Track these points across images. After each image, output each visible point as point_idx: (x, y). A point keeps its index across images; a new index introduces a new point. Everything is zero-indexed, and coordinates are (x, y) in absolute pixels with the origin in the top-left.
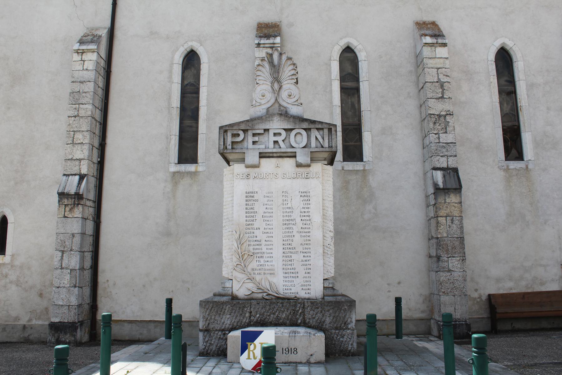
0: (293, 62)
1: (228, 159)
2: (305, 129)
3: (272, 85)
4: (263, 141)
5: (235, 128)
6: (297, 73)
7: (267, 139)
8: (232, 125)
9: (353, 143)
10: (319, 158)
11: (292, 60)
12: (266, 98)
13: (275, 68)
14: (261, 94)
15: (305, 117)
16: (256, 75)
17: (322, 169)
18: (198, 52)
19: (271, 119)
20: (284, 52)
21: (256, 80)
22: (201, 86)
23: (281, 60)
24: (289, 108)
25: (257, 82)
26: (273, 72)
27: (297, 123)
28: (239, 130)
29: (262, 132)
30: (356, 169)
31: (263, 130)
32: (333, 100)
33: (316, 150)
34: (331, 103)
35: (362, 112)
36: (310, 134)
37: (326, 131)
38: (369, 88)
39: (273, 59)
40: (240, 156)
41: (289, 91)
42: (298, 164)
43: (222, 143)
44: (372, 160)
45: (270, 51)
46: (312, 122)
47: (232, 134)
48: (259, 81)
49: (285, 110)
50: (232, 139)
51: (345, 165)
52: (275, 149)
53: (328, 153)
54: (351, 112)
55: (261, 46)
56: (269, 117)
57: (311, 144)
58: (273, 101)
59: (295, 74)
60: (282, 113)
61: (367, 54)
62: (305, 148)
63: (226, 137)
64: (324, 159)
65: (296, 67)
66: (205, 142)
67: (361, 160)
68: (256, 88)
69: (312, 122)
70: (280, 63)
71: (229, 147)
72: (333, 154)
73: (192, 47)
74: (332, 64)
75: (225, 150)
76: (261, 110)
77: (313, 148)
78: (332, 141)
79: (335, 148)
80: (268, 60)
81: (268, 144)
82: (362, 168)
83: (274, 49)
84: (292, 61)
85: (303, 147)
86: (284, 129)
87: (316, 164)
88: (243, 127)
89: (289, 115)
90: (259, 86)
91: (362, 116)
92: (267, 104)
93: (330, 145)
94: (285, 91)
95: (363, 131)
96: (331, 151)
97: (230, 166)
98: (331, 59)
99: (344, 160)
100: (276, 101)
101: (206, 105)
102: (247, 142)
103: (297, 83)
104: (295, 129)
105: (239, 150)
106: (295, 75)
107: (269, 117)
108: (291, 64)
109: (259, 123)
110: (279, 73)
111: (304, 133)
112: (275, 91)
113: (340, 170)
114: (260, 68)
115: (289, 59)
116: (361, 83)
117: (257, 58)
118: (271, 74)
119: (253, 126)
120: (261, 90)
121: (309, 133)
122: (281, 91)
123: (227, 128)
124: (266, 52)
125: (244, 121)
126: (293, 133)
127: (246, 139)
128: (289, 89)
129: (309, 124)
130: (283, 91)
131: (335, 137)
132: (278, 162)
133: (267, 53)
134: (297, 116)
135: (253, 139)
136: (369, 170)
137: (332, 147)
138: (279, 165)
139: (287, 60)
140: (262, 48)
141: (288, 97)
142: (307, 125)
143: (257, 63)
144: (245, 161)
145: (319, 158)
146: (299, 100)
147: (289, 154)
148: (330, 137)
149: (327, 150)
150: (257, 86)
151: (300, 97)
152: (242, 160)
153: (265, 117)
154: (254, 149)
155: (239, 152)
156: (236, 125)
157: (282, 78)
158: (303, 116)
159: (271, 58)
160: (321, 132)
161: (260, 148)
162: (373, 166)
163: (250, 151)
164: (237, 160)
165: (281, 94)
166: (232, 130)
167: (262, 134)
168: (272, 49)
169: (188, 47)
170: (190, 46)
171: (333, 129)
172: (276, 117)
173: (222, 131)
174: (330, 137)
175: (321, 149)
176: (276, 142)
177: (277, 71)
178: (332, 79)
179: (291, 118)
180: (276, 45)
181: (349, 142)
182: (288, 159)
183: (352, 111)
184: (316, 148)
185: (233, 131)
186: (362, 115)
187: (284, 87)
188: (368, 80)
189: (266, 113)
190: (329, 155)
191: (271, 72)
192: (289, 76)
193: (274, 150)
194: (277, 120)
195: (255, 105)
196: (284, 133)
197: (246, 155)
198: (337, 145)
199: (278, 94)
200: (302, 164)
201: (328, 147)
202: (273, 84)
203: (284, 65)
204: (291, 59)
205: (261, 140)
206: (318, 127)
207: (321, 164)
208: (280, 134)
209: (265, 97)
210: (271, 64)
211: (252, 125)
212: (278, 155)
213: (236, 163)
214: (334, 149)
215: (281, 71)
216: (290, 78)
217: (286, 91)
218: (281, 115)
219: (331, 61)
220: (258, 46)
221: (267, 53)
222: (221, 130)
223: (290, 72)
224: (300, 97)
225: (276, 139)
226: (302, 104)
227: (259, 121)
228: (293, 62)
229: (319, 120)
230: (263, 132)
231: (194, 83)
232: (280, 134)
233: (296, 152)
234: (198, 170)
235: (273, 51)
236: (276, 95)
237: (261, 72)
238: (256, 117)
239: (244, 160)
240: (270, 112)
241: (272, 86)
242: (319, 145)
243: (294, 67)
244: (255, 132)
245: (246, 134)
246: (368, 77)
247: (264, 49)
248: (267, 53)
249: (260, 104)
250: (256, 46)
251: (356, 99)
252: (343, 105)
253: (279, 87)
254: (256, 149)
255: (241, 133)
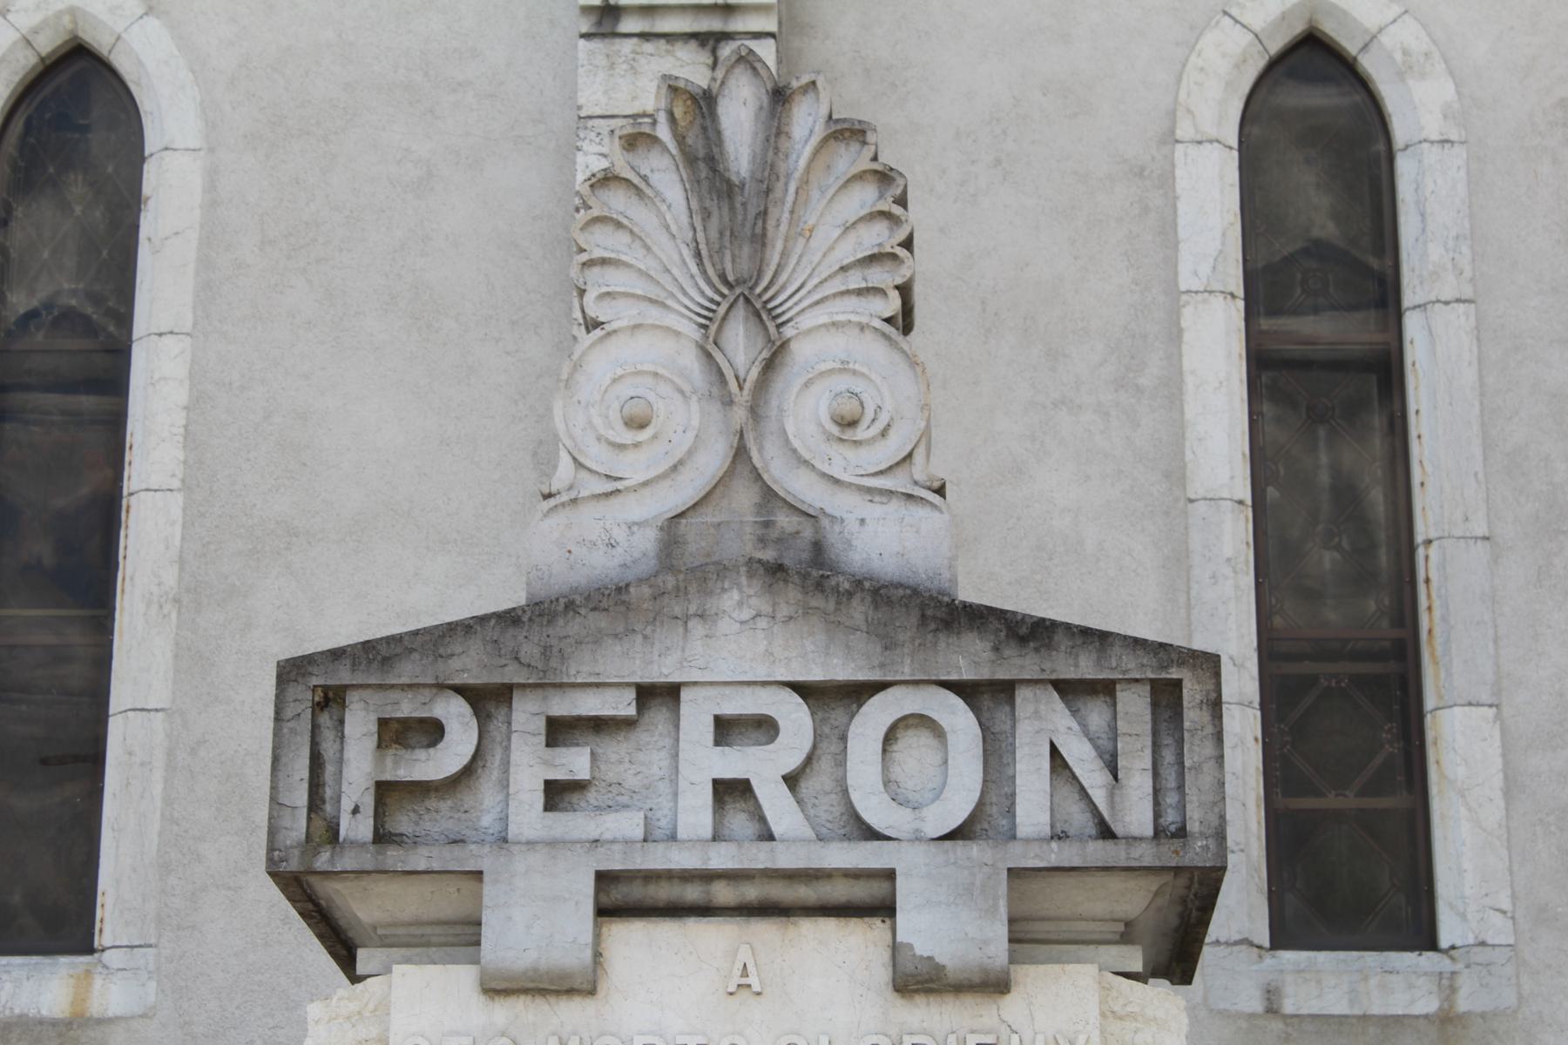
0: (875, 159)
1: (342, 923)
2: (965, 690)
3: (706, 337)
4: (632, 782)
5: (406, 671)
6: (908, 244)
7: (665, 763)
8: (384, 650)
9: (1348, 801)
10: (1081, 926)
11: (864, 143)
12: (655, 437)
13: (732, 208)
14: (616, 406)
15: (967, 593)
16: (584, 257)
17: (1103, 1015)
18: (122, 63)
19: (693, 609)
20: (805, 79)
21: (582, 292)
22: (140, 326)
23: (784, 144)
24: (842, 520)
25: (591, 313)
26: (714, 234)
27: (902, 637)
28: (441, 687)
29: (622, 705)
30: (1376, 1009)
31: (631, 695)
32: (1189, 456)
33: (1056, 855)
34: (1177, 474)
35: (1421, 552)
36: (1007, 727)
37: (1135, 706)
38: (1480, 360)
39: (719, 133)
40: (443, 902)
41: (842, 383)
42: (910, 968)
43: (301, 797)
44: (1511, 941)
45: (692, 67)
46: (1023, 631)
47: (383, 723)
48: (606, 303)
49: (808, 533)
50: (379, 762)
51: (1289, 978)
52: (722, 847)
53: (1154, 888)
54: (1338, 548)
55: (629, 25)
56: (680, 592)
57: (1011, 811)
58: (712, 461)
59: (894, 256)
60: (787, 562)
61: (1458, 93)
62: (1053, 769)
63: (329, 748)
64: (1121, 927)
65: (902, 201)
66: (158, 775)
67: (1424, 936)
68: (584, 354)
69: (1023, 631)
70: (772, 166)
71: (356, 828)
72: (1189, 888)
73: (75, 22)
74: (1178, 173)
75: (317, 853)
76: (620, 534)
77: (1027, 841)
78: (1181, 787)
79: (1212, 844)
80: (680, 139)
81: (666, 803)
82: (1427, 1004)
83: (727, 50)
84: (868, 152)
85: (951, 836)
86: (798, 687)
87: (1057, 967)
88: (470, 665)
89: (837, 571)
90: (601, 340)
91: (1427, 581)
92: (667, 483)
93: (1170, 817)
94: (807, 384)
95: (1430, 702)
96: (1177, 870)
97: (355, 979)
98: (1173, 132)
99: (1283, 936)
100: (739, 467)
101: (176, 484)
102: (504, 784)
103: (905, 321)
104: (881, 686)
105: (435, 851)
106: (889, 265)
107: (677, 588)
108: (860, 177)
109: (597, 640)
110: (760, 241)
111: (957, 717)
112: (733, 385)
113: (1252, 1016)
114: (616, 201)
115: (847, 132)
116: (1413, 325)
117: (590, 123)
118: (704, 252)
119: (554, 663)
120: (620, 372)
121: (1001, 717)
122: (779, 383)
123: (343, 676)
124: (665, 77)
125: (483, 619)
126: (876, 715)
127: (495, 760)
128: (843, 370)
129: (996, 649)
130: (798, 383)
131: (1209, 749)
132: (744, 955)
133: (674, 90)
134: (900, 585)
135: (548, 763)
136: (1483, 1016)
137: (1181, 832)
138: (753, 980)
139: (825, 140)
140: (635, 40)
141: (835, 430)
142: (988, 655)
143: (592, 158)
144: (478, 943)
145: (1081, 926)
146: (919, 457)
147: (839, 892)
148: (1168, 756)
149: (1146, 855)
150: (586, 339)
151: (926, 434)
152: (458, 929)
153: (646, 591)
154: (552, 844)
155: (436, 866)
156: (412, 650)
157: (783, 288)
158: (954, 580)
159: (704, 129)
160: (1096, 714)
161: (608, 836)
162: (1518, 985)
163: (521, 862)
164: (419, 931)
165: (781, 410)
166: (381, 687)
167: (627, 724)
168: (714, 52)
169: (45, 22)
170: (59, 15)
171: (1192, 692)
172: (735, 595)
173: (302, 699)
174: (1168, 756)
175: (1098, 852)
176: (731, 792)
177: (748, 230)
178: (1183, 288)
179: (855, 602)
180: (738, 24)
181: (1317, 793)
182: (829, 925)
183: (1345, 544)
184: (1054, 845)
185: (394, 695)
186: (1421, 576)
187: (803, 352)
188: (1468, 292)
189: (653, 562)
190: (1156, 894)
191: (700, 236)
192: (843, 269)
193: (721, 858)
194: (746, 614)
195: (573, 495)
196: (795, 716)
197: (488, 890)
198: (1222, 817)
199: (755, 412)
200: (944, 967)
201: (1149, 832)
202: (713, 328)
203: (805, 181)
204: (863, 132)
205: (610, 773)
206: (1068, 673)
207: (1092, 969)
208: (764, 727)
209: (644, 435)
210: (704, 172)
211: (546, 651)
212: (751, 893)
213: (408, 961)
214: (1197, 853)
215: (783, 228)
216: (855, 280)
217: (816, 388)
218: (776, 571)
219: (1179, 146)
220: (599, 23)
221: (674, 90)
222: (294, 691)
223: (852, 237)
224: (926, 434)
225: (734, 763)
226: (940, 491)
227: (600, 621)
228: (875, 159)
229: (1076, 620)
230: (631, 711)
231: (89, 310)
232: (764, 727)
233: (890, 875)
234: (95, 1008)
235: (720, 74)
236: (740, 415)
237: (624, 238)
238: (575, 590)
239: (470, 930)
240: (692, 548)
241: (711, 347)
242: (1079, 819)
243: (881, 196)
244: (563, 706)
245: (497, 726)
246: (1468, 273)
247: (648, 47)
248: (674, 89)
249: (609, 486)
250: (584, 30)
251: (1378, 443)
252: (1272, 493)
253: (766, 354)
254: (574, 842)
255: (455, 714)
